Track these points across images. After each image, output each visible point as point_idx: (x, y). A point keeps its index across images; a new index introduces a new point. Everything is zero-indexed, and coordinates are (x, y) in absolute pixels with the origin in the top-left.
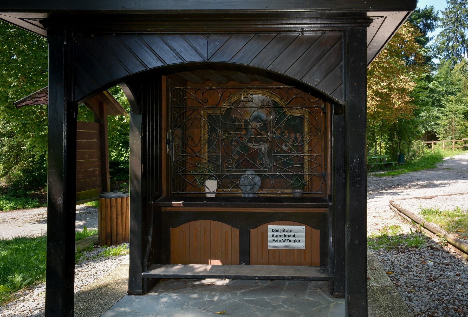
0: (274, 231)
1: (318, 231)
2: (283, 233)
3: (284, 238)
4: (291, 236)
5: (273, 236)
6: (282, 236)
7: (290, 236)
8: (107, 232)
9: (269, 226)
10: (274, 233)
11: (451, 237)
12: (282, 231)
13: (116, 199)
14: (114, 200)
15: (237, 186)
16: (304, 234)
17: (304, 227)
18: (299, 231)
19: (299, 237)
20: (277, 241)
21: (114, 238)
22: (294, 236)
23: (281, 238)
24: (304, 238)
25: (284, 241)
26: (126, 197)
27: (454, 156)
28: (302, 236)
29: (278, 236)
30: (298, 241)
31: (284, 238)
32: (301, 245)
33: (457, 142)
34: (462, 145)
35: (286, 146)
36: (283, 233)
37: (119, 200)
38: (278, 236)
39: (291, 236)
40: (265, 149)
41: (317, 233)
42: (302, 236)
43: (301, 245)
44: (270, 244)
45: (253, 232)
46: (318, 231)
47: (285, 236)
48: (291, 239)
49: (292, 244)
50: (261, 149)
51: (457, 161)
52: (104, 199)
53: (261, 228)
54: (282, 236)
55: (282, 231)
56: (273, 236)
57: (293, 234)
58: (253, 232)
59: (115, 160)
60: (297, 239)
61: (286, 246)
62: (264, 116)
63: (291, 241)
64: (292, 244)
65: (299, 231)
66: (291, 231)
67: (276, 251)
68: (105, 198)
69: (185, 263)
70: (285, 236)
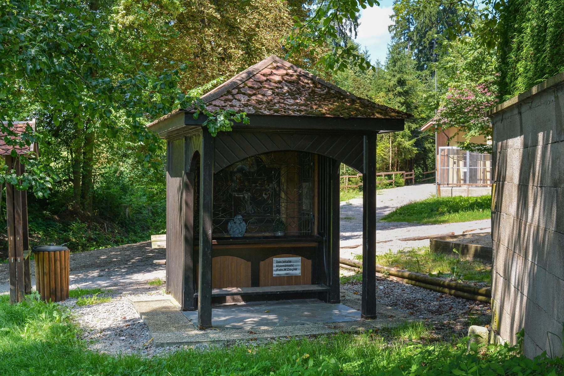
0: (278, 262)
1: (310, 261)
2: (284, 264)
3: (285, 268)
4: (290, 266)
5: (277, 266)
6: (284, 266)
7: (289, 265)
8: (51, 288)
9: (274, 259)
10: (278, 264)
11: (393, 270)
12: (284, 262)
13: (55, 252)
14: (63, 251)
15: (227, 231)
16: (300, 263)
17: (300, 258)
18: (297, 262)
19: (296, 266)
20: (280, 270)
21: (59, 294)
22: (293, 266)
23: (283, 268)
24: (300, 267)
25: (285, 270)
26: (54, 251)
27: (349, 200)
28: (298, 266)
29: (281, 266)
30: (296, 269)
31: (285, 268)
32: (298, 272)
33: (351, 179)
34: (357, 184)
35: (266, 194)
36: (284, 264)
37: (63, 252)
38: (281, 266)
39: (290, 266)
40: (248, 197)
41: (309, 262)
42: (298, 266)
43: (298, 272)
44: (274, 273)
45: (262, 263)
46: (310, 261)
47: (286, 266)
48: (290, 268)
49: (291, 272)
50: (244, 197)
51: (356, 207)
52: (47, 252)
53: (267, 261)
54: (284, 266)
55: (284, 262)
56: (277, 266)
57: (292, 264)
58: (262, 263)
59: (118, 207)
60: (295, 267)
61: (287, 274)
62: (247, 168)
63: (290, 270)
64: (291, 272)
65: (297, 262)
66: (290, 262)
67: (280, 277)
68: (43, 251)
69: (220, 288)
70: (286, 266)
